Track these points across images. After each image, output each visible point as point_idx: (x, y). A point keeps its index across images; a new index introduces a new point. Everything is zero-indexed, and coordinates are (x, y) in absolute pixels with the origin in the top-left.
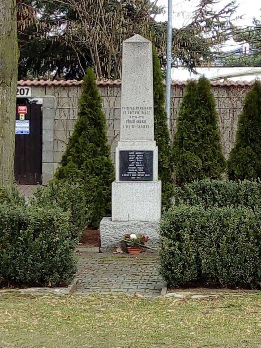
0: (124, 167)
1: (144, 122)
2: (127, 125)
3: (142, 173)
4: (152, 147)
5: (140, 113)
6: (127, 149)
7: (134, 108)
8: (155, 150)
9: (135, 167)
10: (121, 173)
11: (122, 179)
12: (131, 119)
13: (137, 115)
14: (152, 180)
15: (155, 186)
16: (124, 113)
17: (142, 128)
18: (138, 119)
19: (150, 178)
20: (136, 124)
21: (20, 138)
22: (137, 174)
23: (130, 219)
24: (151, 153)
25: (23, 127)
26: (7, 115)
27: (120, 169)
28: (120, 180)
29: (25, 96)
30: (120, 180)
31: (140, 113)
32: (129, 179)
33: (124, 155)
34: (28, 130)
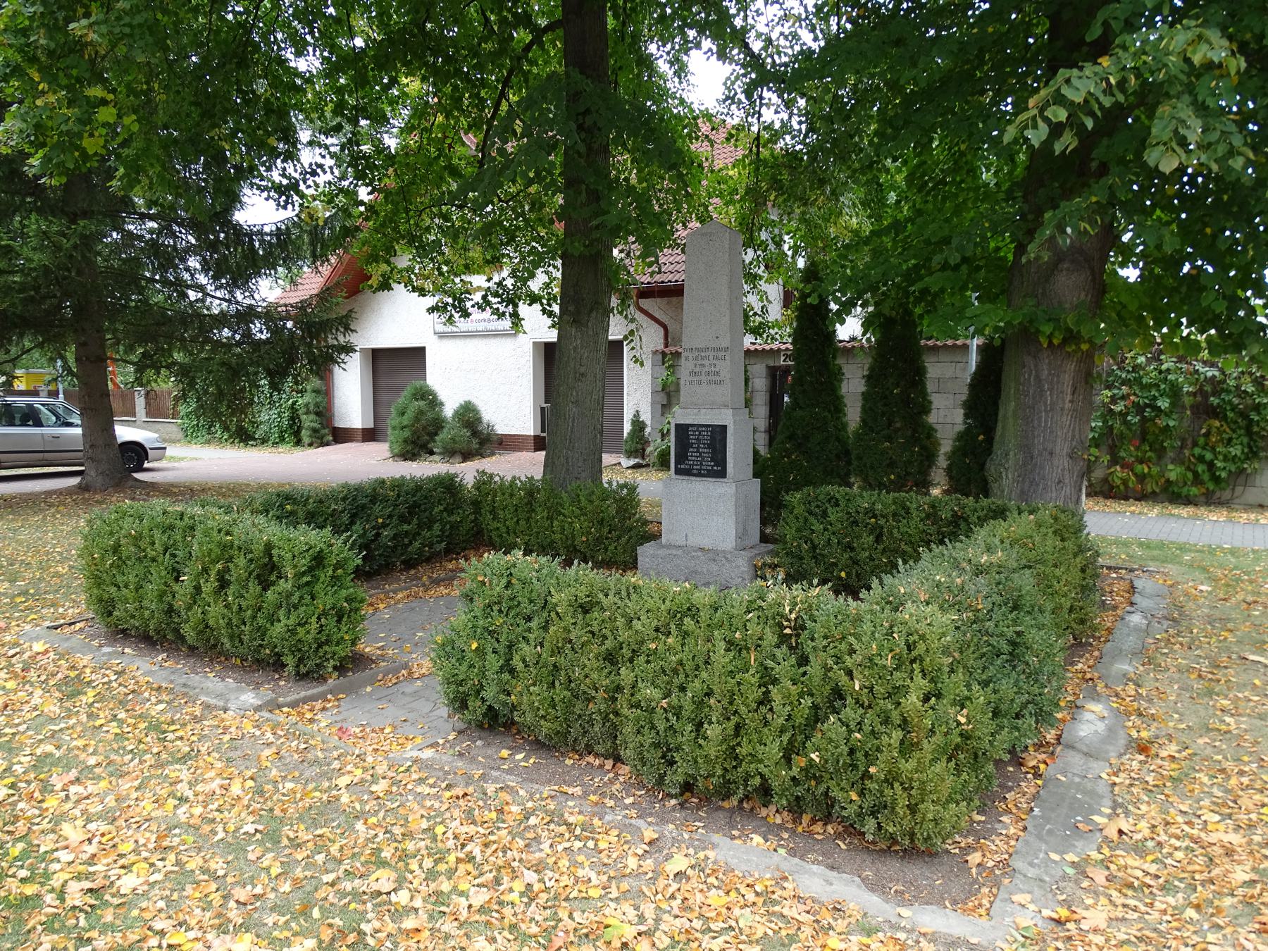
1: (717, 373)
7: (699, 350)
12: (697, 369)
13: (706, 362)
18: (707, 369)
20: (704, 378)
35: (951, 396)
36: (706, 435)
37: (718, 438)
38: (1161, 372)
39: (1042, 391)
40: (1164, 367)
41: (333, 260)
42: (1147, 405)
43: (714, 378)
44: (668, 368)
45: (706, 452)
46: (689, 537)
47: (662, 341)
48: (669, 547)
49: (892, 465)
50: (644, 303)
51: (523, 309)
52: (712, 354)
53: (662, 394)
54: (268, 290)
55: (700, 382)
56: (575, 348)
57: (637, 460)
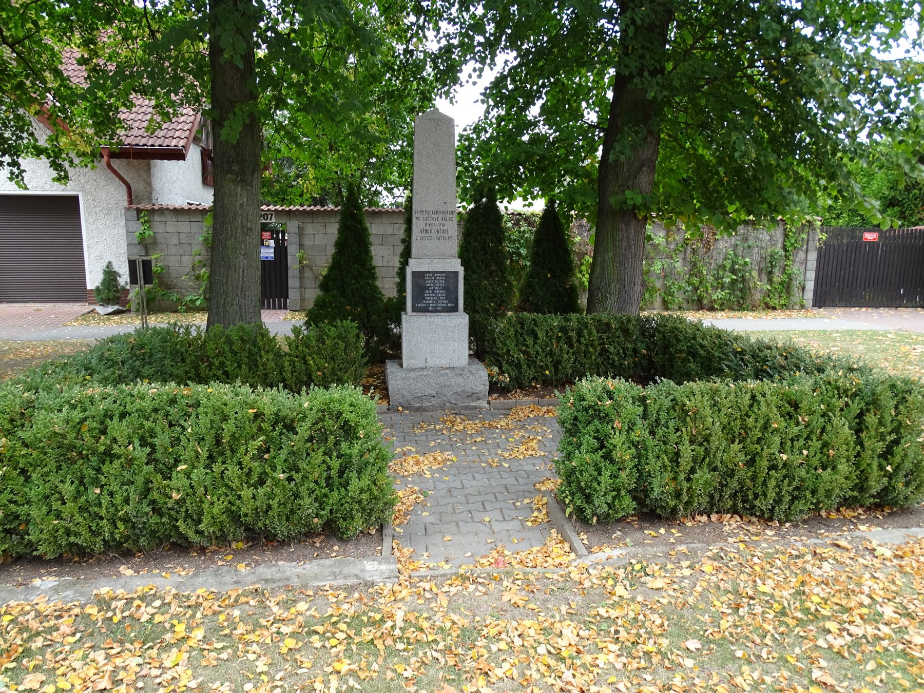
0: (420, 290)
1: (445, 231)
2: (422, 235)
3: (444, 303)
4: (456, 266)
5: (440, 219)
6: (423, 270)
7: (430, 212)
8: (461, 270)
9: (430, 295)
10: (415, 300)
12: (427, 228)
13: (436, 222)
14: (457, 311)
15: (460, 321)
16: (418, 219)
17: (442, 241)
18: (436, 228)
19: (455, 309)
20: (434, 235)
21: (265, 263)
22: (437, 302)
23: (428, 365)
24: (456, 274)
25: (268, 252)
26: (249, 225)
27: (413, 297)
28: (413, 311)
29: (268, 221)
30: (413, 311)
31: (440, 219)
32: (425, 310)
34: (273, 255)
35: (391, 248)
36: (441, 282)
37: (452, 281)
38: (520, 232)
39: (630, 246)
40: (522, 229)
41: (699, 143)
42: (514, 253)
43: (442, 234)
44: (144, 223)
45: (442, 294)
46: (429, 359)
47: (126, 197)
48: (412, 370)
49: (493, 296)
50: (115, 163)
51: (26, 162)
52: (440, 216)
53: (140, 247)
54: (586, 162)
55: (430, 238)
56: (242, 205)
57: (116, 307)
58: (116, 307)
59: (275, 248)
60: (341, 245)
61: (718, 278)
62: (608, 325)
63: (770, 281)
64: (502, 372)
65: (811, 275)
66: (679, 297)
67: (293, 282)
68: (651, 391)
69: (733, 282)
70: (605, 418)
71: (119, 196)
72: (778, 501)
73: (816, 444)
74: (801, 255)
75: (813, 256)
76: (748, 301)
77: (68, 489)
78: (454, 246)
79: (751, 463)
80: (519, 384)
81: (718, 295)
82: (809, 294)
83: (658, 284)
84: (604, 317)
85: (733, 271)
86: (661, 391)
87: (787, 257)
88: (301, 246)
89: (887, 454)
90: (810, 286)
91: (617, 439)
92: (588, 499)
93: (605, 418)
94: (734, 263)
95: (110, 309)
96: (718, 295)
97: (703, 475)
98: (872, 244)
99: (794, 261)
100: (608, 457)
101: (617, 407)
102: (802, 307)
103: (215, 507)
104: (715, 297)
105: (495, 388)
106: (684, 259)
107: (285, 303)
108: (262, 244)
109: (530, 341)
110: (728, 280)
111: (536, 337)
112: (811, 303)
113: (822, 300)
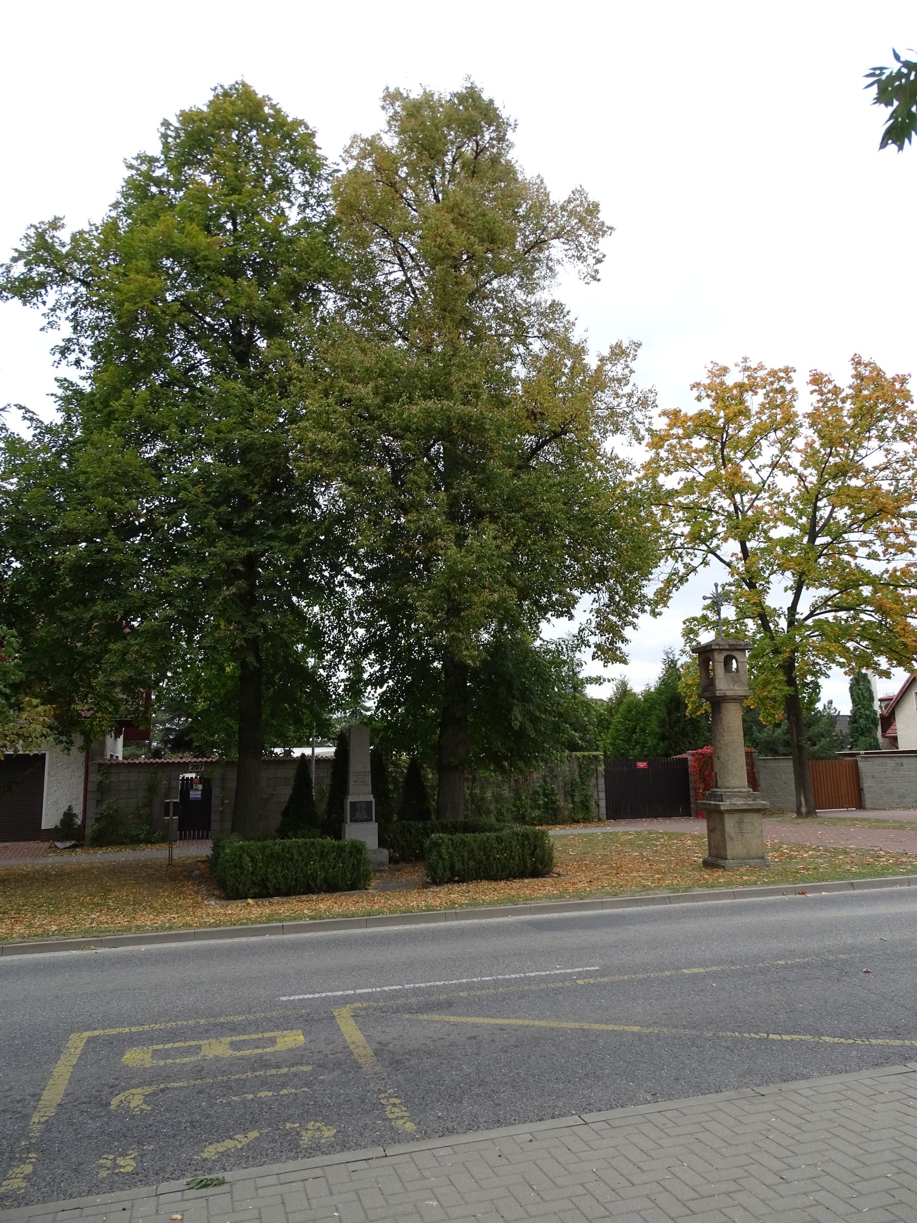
3: (365, 817)
4: (371, 798)
8: (373, 800)
11: (351, 821)
33: (353, 804)
57: (73, 842)
58: (73, 842)
59: (202, 791)
60: (296, 789)
61: (534, 800)
62: (446, 826)
63: (573, 802)
64: (394, 852)
65: (602, 795)
66: (508, 816)
67: (214, 817)
68: (454, 837)
69: (546, 804)
70: (440, 845)
71: (77, 756)
72: (498, 872)
73: (508, 852)
74: (593, 780)
75: (602, 781)
76: (560, 817)
77: (279, 869)
78: (369, 788)
79: (487, 859)
80: (404, 859)
81: (537, 813)
82: (603, 810)
83: (492, 807)
84: (444, 821)
85: (546, 795)
86: (458, 836)
87: (583, 783)
88: (223, 788)
89: (532, 854)
90: (603, 803)
91: (443, 851)
92: (436, 873)
93: (440, 845)
94: (545, 790)
95: (68, 844)
96: (537, 813)
97: (472, 863)
98: (643, 769)
99: (589, 786)
100: (441, 857)
101: (443, 841)
102: (599, 820)
103: (321, 875)
104: (533, 815)
105: (392, 860)
106: (510, 787)
107: (207, 834)
108: (192, 788)
109: (408, 835)
110: (541, 802)
111: (411, 833)
112: (605, 817)
113: (616, 813)
